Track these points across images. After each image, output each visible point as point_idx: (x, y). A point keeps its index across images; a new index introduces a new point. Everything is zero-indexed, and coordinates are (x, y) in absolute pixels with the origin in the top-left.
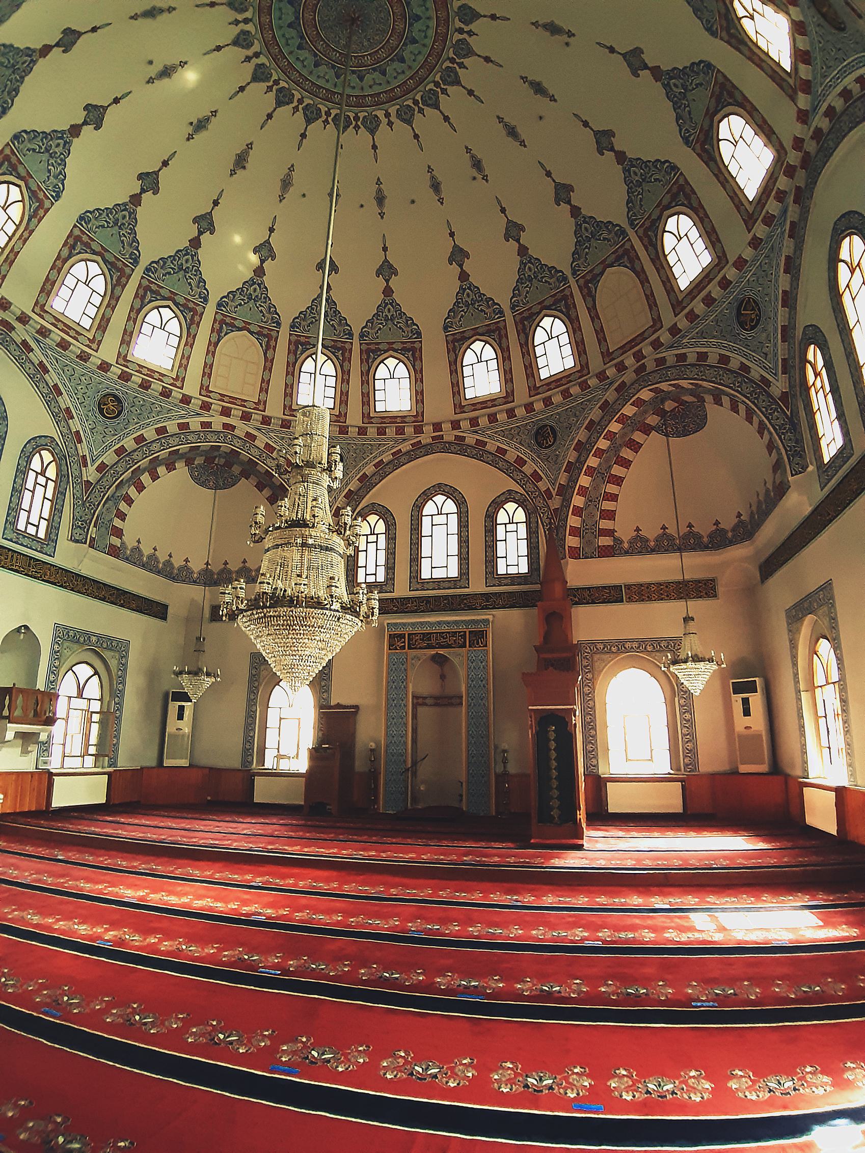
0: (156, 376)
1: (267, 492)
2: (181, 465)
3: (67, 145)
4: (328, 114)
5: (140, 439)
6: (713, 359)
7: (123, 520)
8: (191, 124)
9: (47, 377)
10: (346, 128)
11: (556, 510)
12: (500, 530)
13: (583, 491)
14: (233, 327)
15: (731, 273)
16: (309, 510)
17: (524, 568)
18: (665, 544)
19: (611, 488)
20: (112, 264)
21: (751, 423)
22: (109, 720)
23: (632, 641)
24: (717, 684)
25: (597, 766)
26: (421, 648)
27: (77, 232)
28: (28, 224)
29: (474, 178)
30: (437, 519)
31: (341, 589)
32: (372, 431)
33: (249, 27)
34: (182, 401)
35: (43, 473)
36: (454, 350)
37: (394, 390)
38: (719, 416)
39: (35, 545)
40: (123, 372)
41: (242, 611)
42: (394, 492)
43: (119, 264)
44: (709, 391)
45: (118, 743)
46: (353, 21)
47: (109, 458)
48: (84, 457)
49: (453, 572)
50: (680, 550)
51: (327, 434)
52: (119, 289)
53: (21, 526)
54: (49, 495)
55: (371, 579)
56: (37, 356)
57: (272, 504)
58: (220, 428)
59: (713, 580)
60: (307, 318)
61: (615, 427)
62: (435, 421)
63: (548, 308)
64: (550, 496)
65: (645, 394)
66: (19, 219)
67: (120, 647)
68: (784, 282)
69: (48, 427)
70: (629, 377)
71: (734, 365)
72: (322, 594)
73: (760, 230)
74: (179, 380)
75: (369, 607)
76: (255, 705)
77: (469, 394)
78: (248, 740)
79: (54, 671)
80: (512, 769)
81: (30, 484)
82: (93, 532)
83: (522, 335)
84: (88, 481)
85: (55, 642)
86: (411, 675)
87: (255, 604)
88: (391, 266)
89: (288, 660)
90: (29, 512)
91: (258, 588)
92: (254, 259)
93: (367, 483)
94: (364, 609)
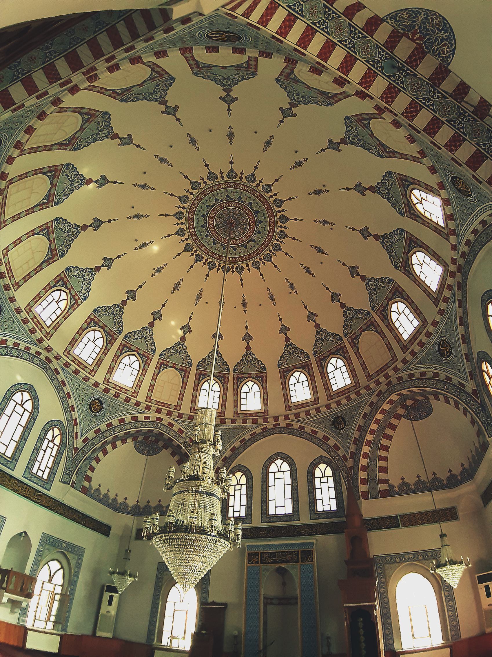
0: (124, 390)
1: (177, 458)
2: (129, 440)
4: (219, 265)
6: (429, 375)
8: (154, 269)
9: (64, 388)
10: (228, 271)
11: (351, 468)
12: (317, 481)
13: (366, 456)
15: (431, 329)
16: (201, 469)
17: (334, 507)
18: (421, 487)
19: (383, 453)
21: (458, 409)
23: (408, 553)
24: (468, 579)
26: (269, 563)
29: (291, 293)
30: (278, 475)
31: (218, 522)
32: (239, 421)
34: (135, 405)
35: (52, 441)
36: (284, 376)
37: (251, 399)
38: (439, 406)
39: (40, 483)
40: (106, 388)
41: (156, 534)
42: (252, 457)
44: (430, 393)
47: (91, 435)
48: (77, 433)
50: (431, 490)
51: (214, 423)
52: (109, 345)
53: (34, 471)
54: (54, 454)
55: (237, 514)
56: (61, 377)
57: (179, 465)
58: (154, 420)
60: (205, 363)
61: (379, 416)
62: (276, 415)
63: (333, 353)
64: (346, 460)
65: (394, 397)
66: (64, 308)
67: (78, 551)
68: (461, 330)
69: (61, 416)
70: (383, 388)
71: (442, 377)
72: (206, 524)
73: (442, 305)
74: (135, 393)
75: (235, 534)
76: (159, 599)
77: (294, 400)
78: (152, 623)
80: (334, 650)
81: (44, 447)
83: (320, 368)
84: (77, 447)
85: (40, 544)
87: (164, 530)
88: (250, 336)
89: (182, 569)
90: (41, 463)
91: (167, 519)
92: (181, 333)
93: (236, 453)
94: (232, 535)
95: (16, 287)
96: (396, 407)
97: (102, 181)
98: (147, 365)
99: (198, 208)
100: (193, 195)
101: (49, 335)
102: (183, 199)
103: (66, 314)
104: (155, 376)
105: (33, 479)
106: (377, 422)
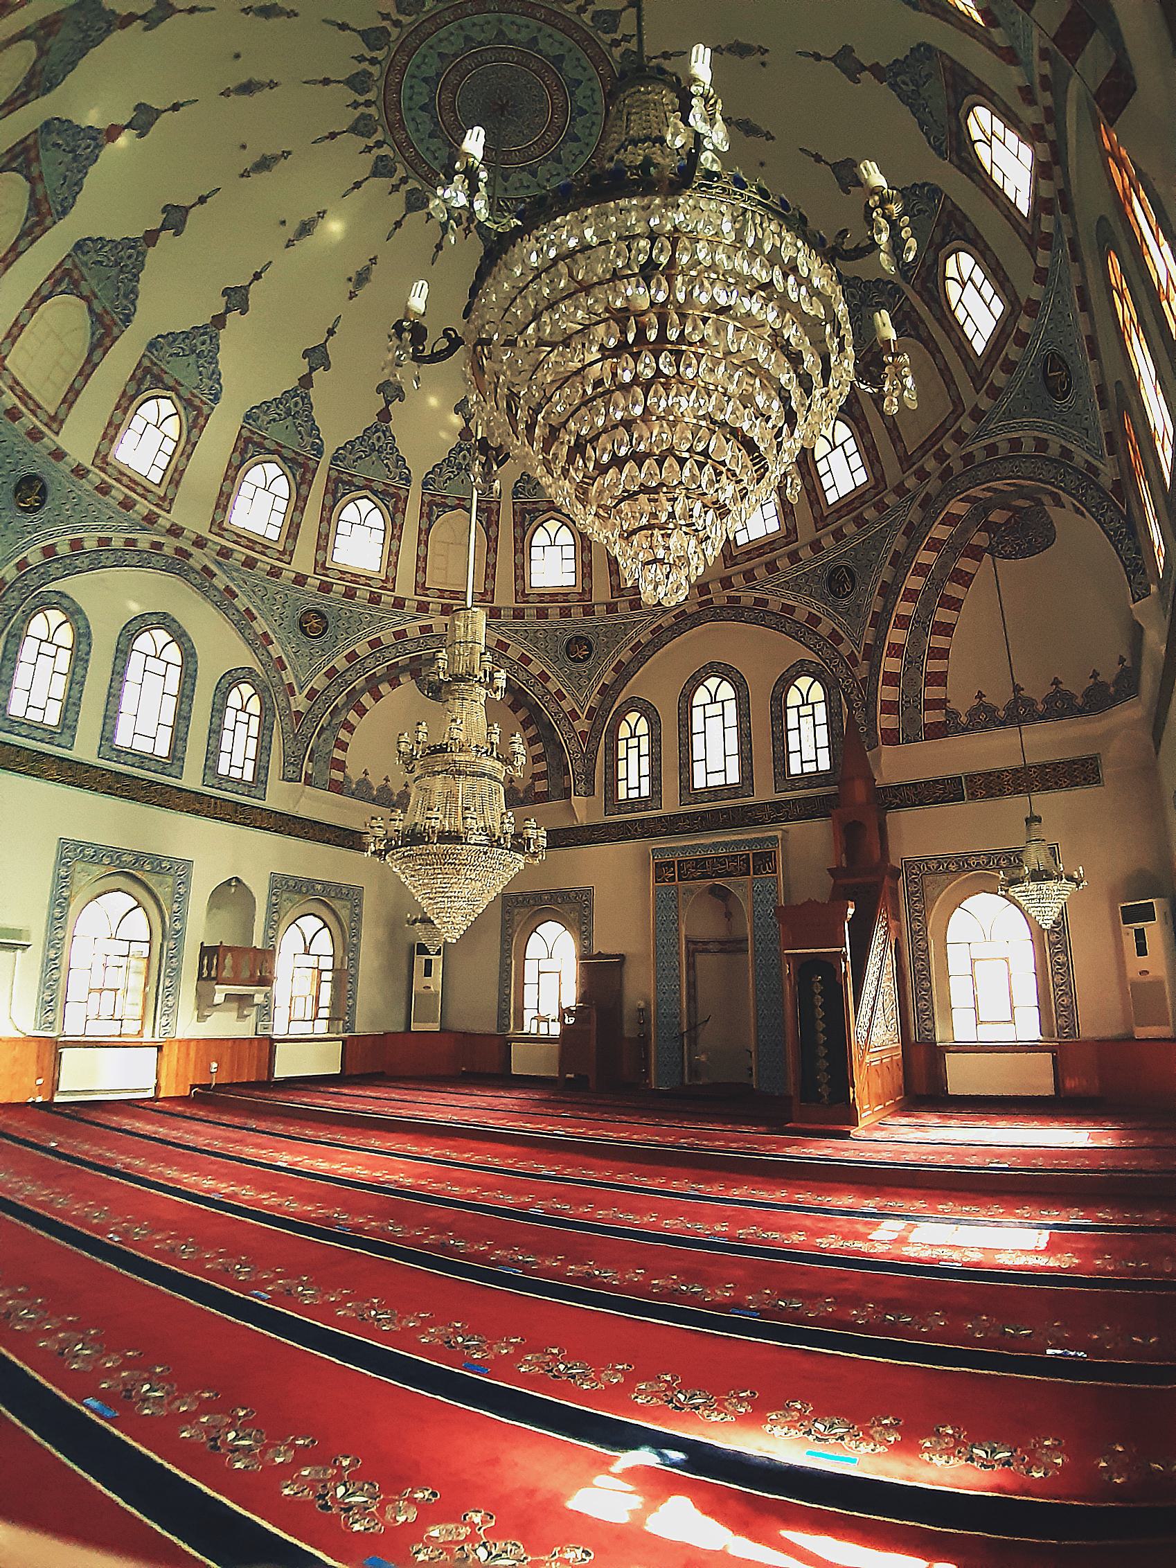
3: (214, 338)
5: (352, 656)
6: (1028, 447)
7: (345, 750)
8: (350, 279)
12: (792, 715)
14: (445, 507)
18: (1019, 713)
19: (938, 641)
20: (292, 460)
22: (343, 979)
25: (933, 1030)
26: (694, 879)
27: (245, 433)
28: (188, 436)
33: (385, 151)
34: (394, 606)
40: (322, 582)
43: (300, 459)
45: (354, 1004)
46: (502, 108)
47: (319, 682)
49: (734, 777)
52: (304, 487)
56: (221, 581)
59: (1094, 758)
64: (855, 662)
65: (957, 507)
67: (352, 895)
69: (245, 658)
70: (933, 486)
71: (1054, 451)
74: (389, 581)
79: (272, 925)
82: (308, 767)
86: (684, 914)
92: (456, 420)
95: (55, 426)
96: (964, 531)
97: (144, 119)
98: (399, 515)
99: (405, 92)
100: (380, 63)
101: (165, 502)
102: (357, 82)
103: (187, 445)
104: (423, 537)
105: (224, 785)
106: (922, 570)
